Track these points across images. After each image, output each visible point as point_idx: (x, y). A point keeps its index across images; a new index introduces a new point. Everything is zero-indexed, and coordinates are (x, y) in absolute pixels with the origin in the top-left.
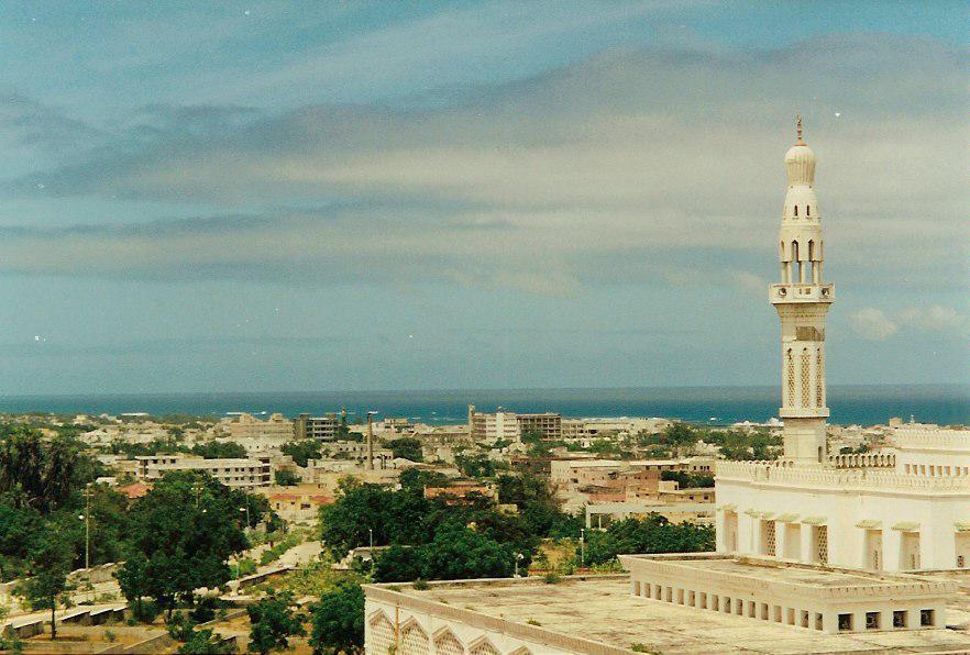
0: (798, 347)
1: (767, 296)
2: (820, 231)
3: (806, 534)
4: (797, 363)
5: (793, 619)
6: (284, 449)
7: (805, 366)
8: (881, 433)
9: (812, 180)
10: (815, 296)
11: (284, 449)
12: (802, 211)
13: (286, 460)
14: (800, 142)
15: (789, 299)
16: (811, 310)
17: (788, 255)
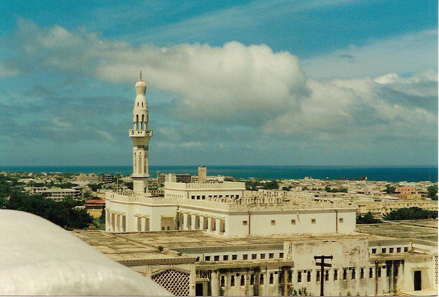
0: (138, 152)
1: (128, 134)
2: (147, 111)
3: (121, 217)
4: (138, 157)
5: (224, 229)
6: (89, 185)
7: (140, 159)
8: (298, 182)
9: (145, 93)
10: (143, 134)
11: (89, 185)
12: (140, 104)
13: (89, 189)
14: (141, 80)
15: (134, 135)
16: (143, 139)
17: (135, 120)
